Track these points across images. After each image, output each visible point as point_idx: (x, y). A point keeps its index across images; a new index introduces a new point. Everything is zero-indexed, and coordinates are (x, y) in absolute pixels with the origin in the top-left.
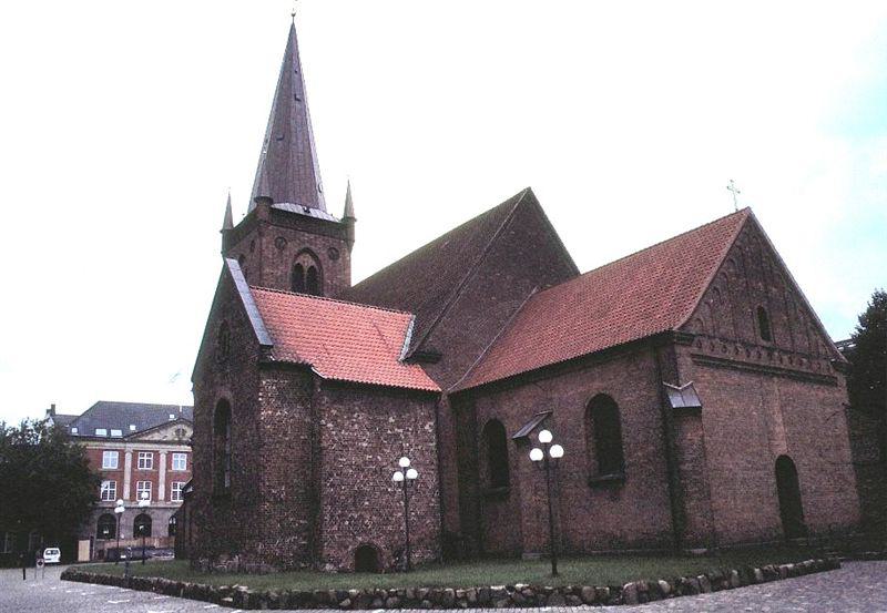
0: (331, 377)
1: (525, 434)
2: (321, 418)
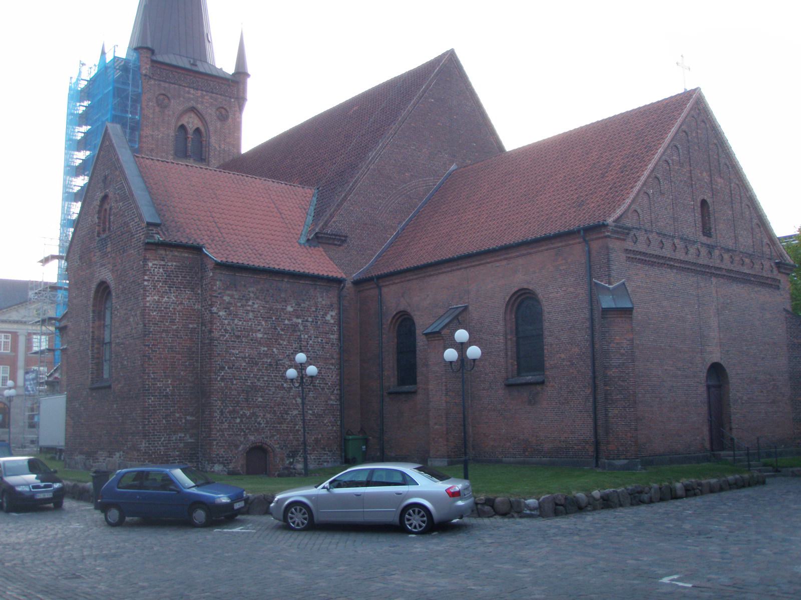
0: (224, 260)
1: (437, 330)
2: (211, 306)
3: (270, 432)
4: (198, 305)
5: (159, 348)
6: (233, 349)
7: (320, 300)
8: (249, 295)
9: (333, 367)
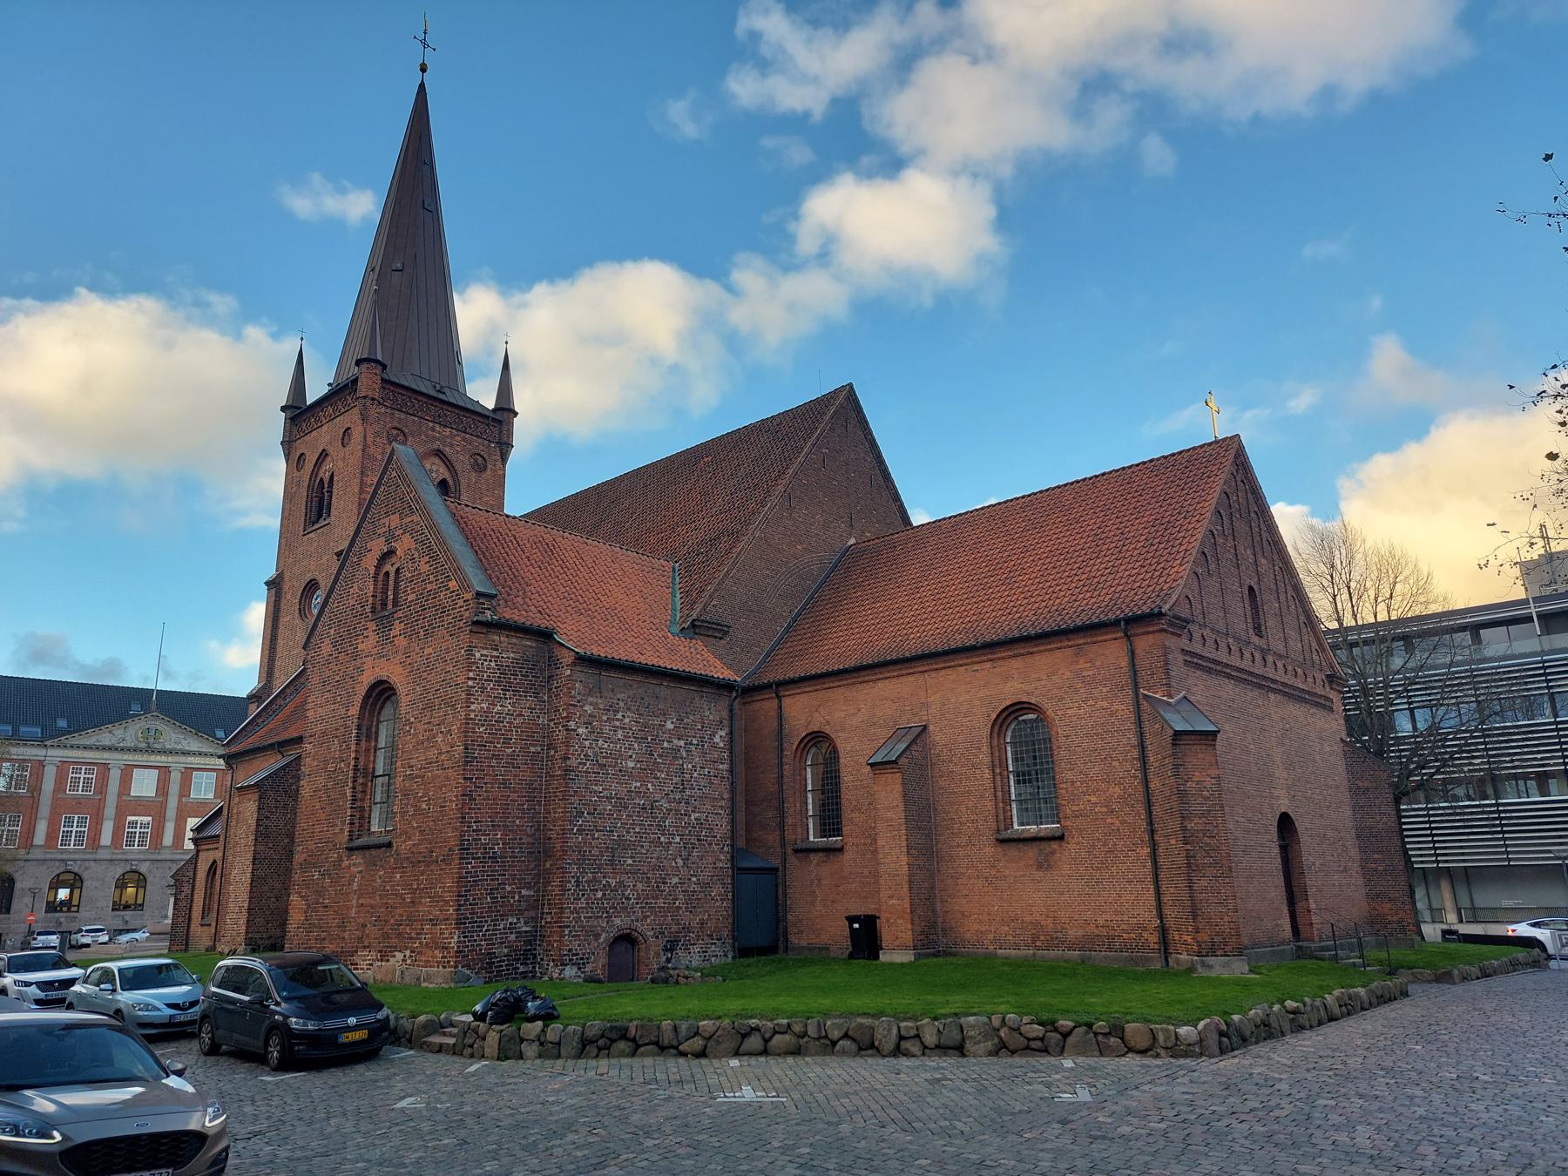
2: (568, 719)
3: (642, 912)
4: (544, 718)
5: (486, 783)
6: (596, 785)
7: (707, 713)
8: (618, 704)
9: (723, 812)
